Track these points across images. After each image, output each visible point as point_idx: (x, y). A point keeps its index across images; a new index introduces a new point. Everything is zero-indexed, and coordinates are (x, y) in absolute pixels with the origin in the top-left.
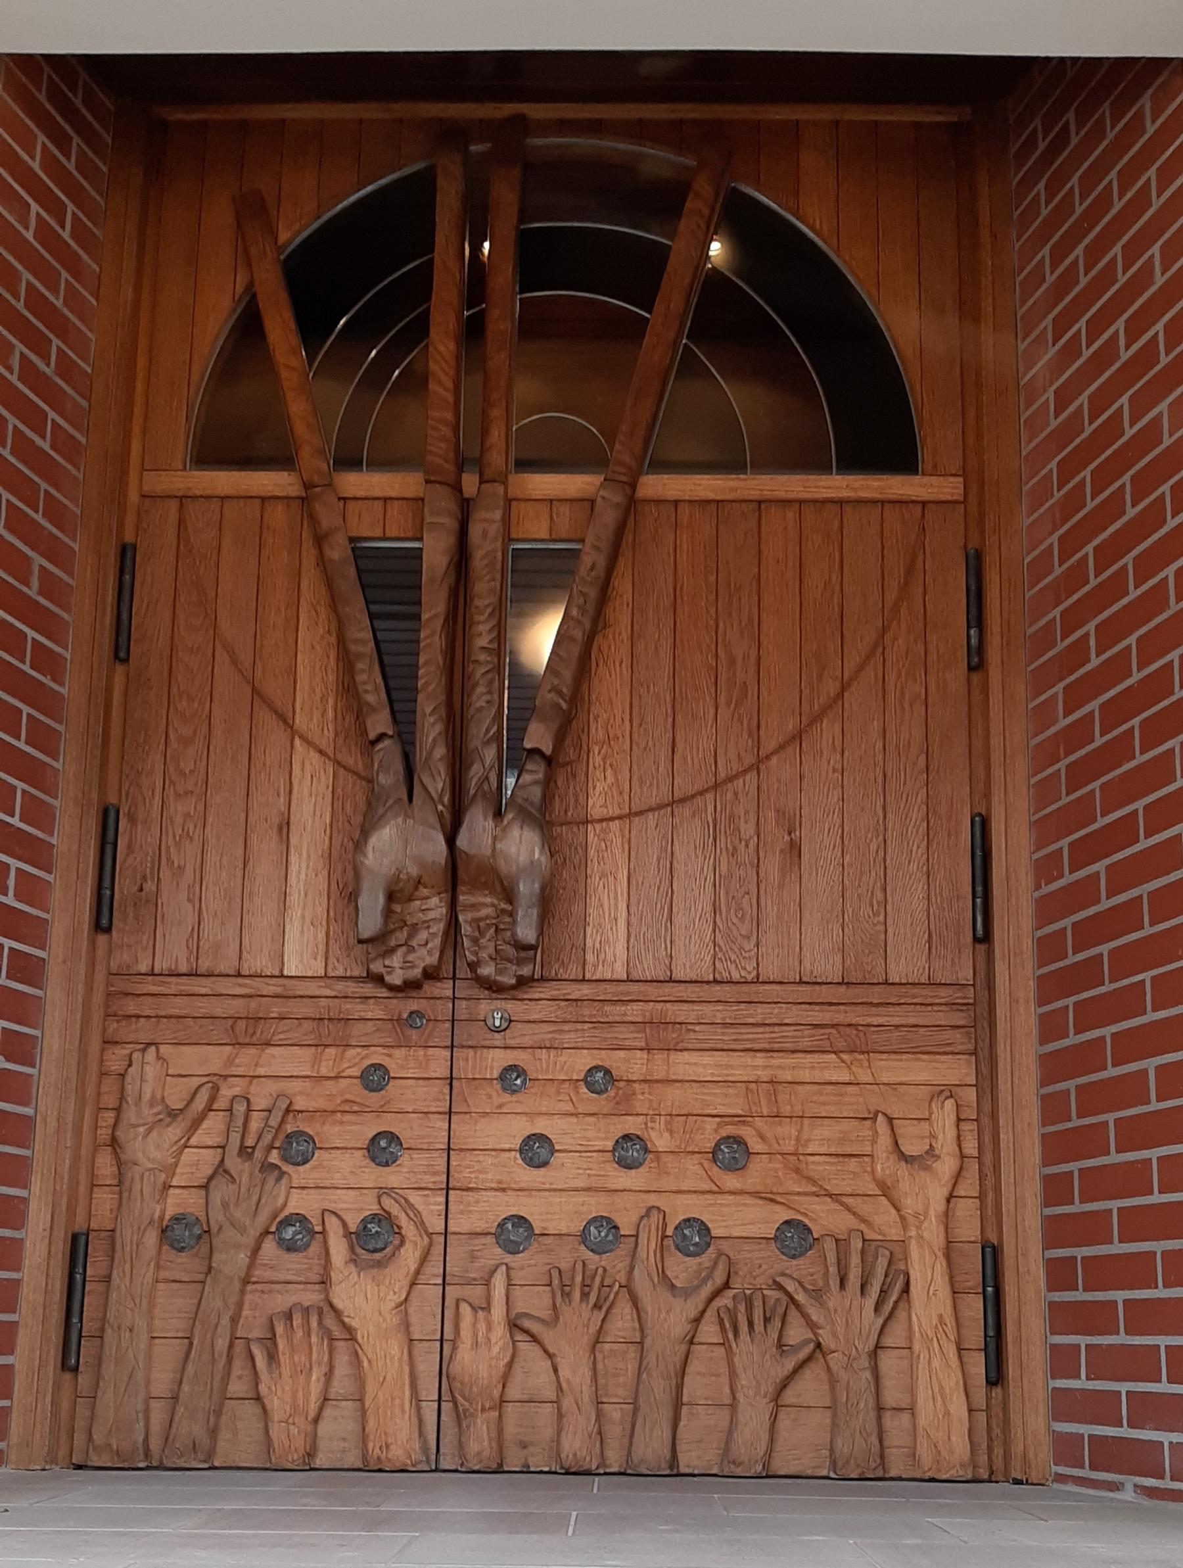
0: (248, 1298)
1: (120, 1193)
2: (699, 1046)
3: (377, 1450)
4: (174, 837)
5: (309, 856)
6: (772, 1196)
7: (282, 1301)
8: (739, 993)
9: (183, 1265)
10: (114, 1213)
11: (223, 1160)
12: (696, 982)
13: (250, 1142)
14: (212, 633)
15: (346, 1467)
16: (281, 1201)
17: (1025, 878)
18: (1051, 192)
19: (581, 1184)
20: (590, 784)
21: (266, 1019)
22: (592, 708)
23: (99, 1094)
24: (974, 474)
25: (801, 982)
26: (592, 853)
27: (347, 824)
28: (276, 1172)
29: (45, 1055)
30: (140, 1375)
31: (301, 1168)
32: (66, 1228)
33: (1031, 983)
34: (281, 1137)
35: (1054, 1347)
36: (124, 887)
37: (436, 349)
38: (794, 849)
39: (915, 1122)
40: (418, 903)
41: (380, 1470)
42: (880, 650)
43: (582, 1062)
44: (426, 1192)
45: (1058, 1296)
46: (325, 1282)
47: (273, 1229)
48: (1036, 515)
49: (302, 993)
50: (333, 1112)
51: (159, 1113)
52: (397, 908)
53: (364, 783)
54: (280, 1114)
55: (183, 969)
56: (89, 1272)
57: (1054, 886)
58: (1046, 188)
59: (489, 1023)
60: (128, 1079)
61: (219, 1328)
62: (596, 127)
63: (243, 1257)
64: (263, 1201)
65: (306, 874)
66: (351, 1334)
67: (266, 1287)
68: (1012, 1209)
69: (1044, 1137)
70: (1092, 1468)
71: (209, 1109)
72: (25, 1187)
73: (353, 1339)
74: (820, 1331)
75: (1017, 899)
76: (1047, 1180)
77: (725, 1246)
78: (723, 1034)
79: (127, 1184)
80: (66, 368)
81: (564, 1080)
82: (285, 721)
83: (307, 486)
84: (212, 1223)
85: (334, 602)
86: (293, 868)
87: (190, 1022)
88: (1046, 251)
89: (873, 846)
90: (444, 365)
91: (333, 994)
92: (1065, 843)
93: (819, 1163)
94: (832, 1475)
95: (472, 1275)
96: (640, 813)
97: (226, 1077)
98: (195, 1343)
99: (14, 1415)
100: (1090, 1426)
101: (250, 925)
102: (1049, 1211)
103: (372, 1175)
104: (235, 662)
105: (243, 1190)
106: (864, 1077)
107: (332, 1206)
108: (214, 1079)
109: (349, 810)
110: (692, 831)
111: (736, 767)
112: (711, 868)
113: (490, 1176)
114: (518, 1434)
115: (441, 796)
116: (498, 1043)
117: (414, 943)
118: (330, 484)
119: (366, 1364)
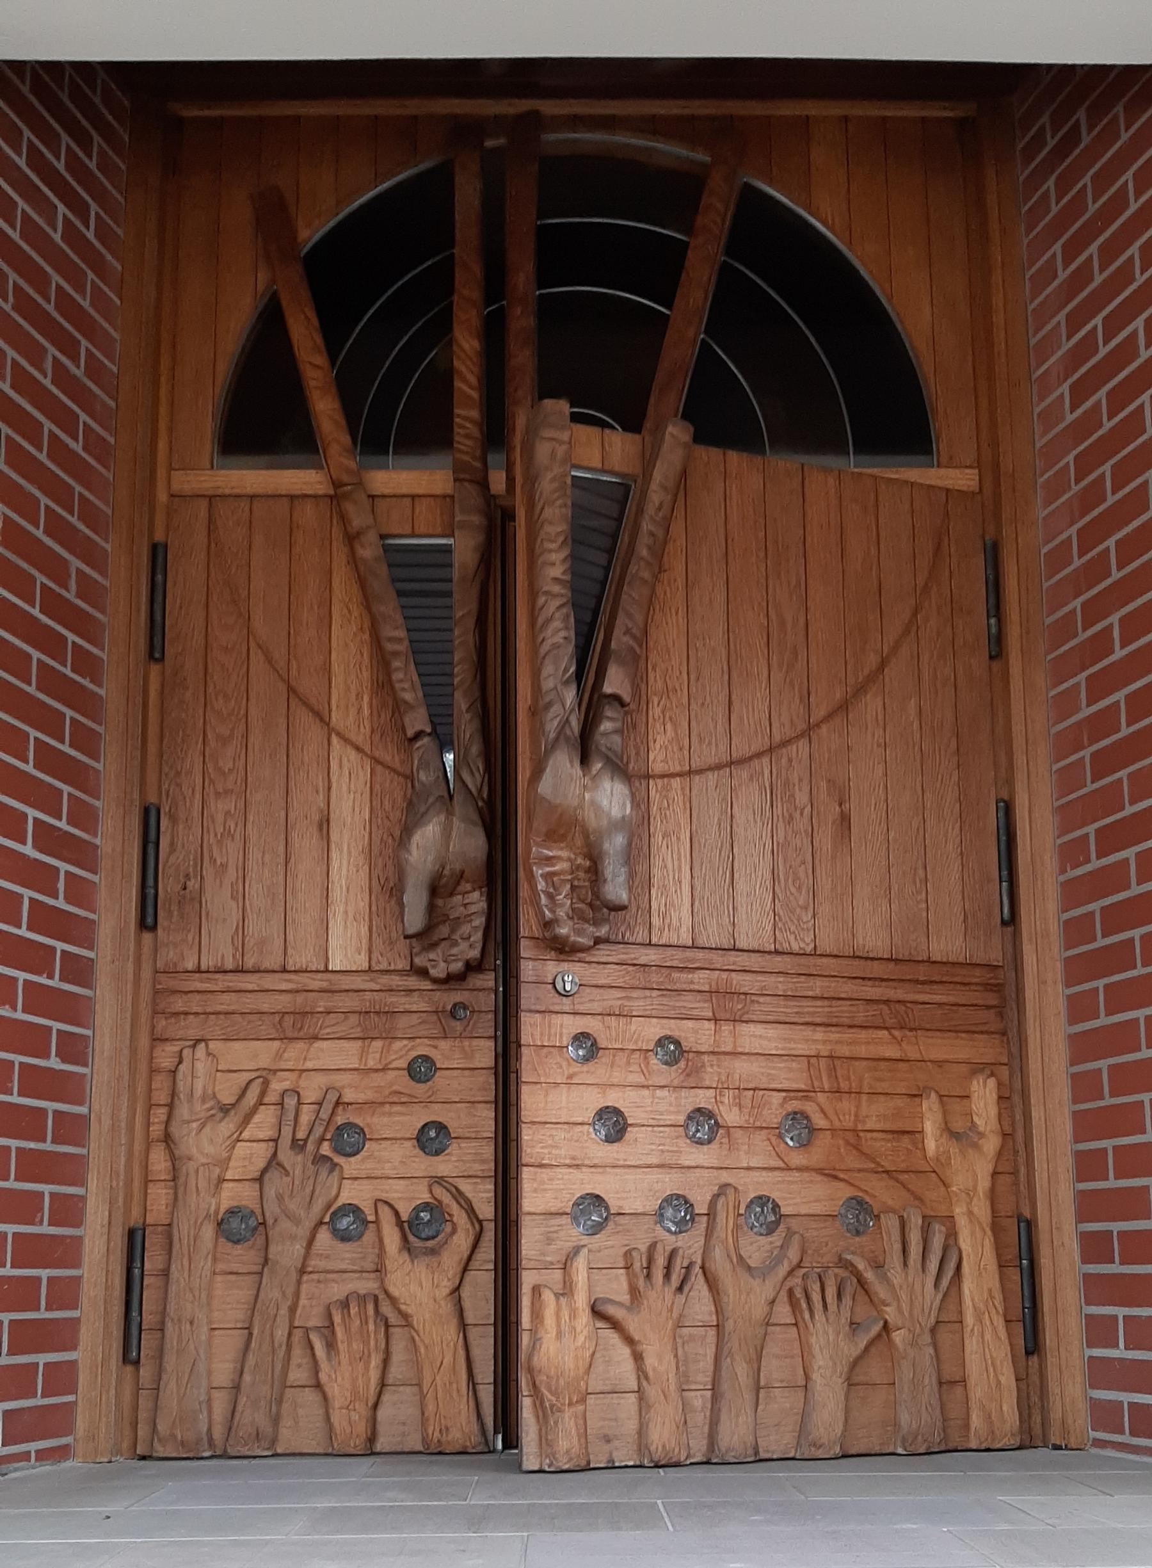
0: (304, 1287)
1: (176, 1188)
2: (763, 1018)
3: (437, 1434)
4: (216, 835)
5: (349, 853)
6: (834, 1173)
7: (337, 1290)
8: (799, 965)
9: (242, 1257)
10: (170, 1208)
11: (275, 1154)
12: (758, 951)
13: (301, 1135)
14: (245, 631)
15: (407, 1450)
16: (334, 1192)
17: (1050, 861)
18: (1063, 187)
19: (654, 1160)
20: (650, 737)
21: (312, 1013)
22: (651, 656)
23: (150, 1090)
24: (991, 468)
25: (854, 957)
26: (654, 809)
27: (386, 821)
28: (328, 1165)
29: (96, 1052)
30: (201, 1367)
31: (352, 1159)
32: (124, 1224)
33: (1058, 964)
34: (332, 1129)
35: (1089, 1317)
36: (168, 886)
37: (460, 346)
38: (845, 820)
39: (958, 1100)
40: (460, 897)
41: (440, 1453)
42: (915, 628)
43: (653, 1030)
44: (475, 1180)
45: (1093, 1269)
46: (379, 1270)
47: (327, 1219)
48: (1053, 506)
49: (347, 988)
50: (382, 1104)
51: (211, 1109)
52: (440, 902)
53: (401, 779)
54: (331, 1106)
55: (229, 964)
56: (147, 1266)
57: (1079, 871)
58: (1056, 184)
59: (559, 986)
60: (180, 1076)
61: (278, 1319)
62: (608, 123)
63: (299, 1248)
64: (317, 1193)
65: (348, 871)
66: (407, 1321)
67: (322, 1276)
68: (1046, 1185)
69: (1076, 1115)
70: (1132, 1434)
71: (260, 1103)
72: (82, 1185)
73: (409, 1325)
74: (887, 1309)
75: (1043, 881)
76: (1079, 1156)
77: (794, 1223)
78: (786, 1007)
79: (181, 1180)
80: (95, 370)
81: (634, 1050)
82: (322, 720)
83: (337, 484)
84: (267, 1215)
85: (367, 601)
86: (335, 864)
87: (238, 1018)
88: (1057, 247)
89: (915, 825)
90: (469, 363)
91: (378, 987)
92: (1091, 829)
93: (875, 1140)
94: (900, 1451)
95: (549, 1259)
96: (700, 772)
97: (275, 1071)
98: (255, 1332)
99: (79, 1410)
100: (1129, 1394)
101: (294, 921)
102: (1082, 1186)
103: (423, 1165)
104: (269, 660)
105: (297, 1182)
106: (913, 1054)
107: (384, 1196)
108: (264, 1073)
109: (387, 805)
110: (750, 796)
111: (789, 733)
112: (769, 834)
113: (563, 1152)
114: (602, 1427)
115: (480, 791)
116: (567, 1009)
117: (456, 937)
118: (360, 484)
119: (422, 1350)
